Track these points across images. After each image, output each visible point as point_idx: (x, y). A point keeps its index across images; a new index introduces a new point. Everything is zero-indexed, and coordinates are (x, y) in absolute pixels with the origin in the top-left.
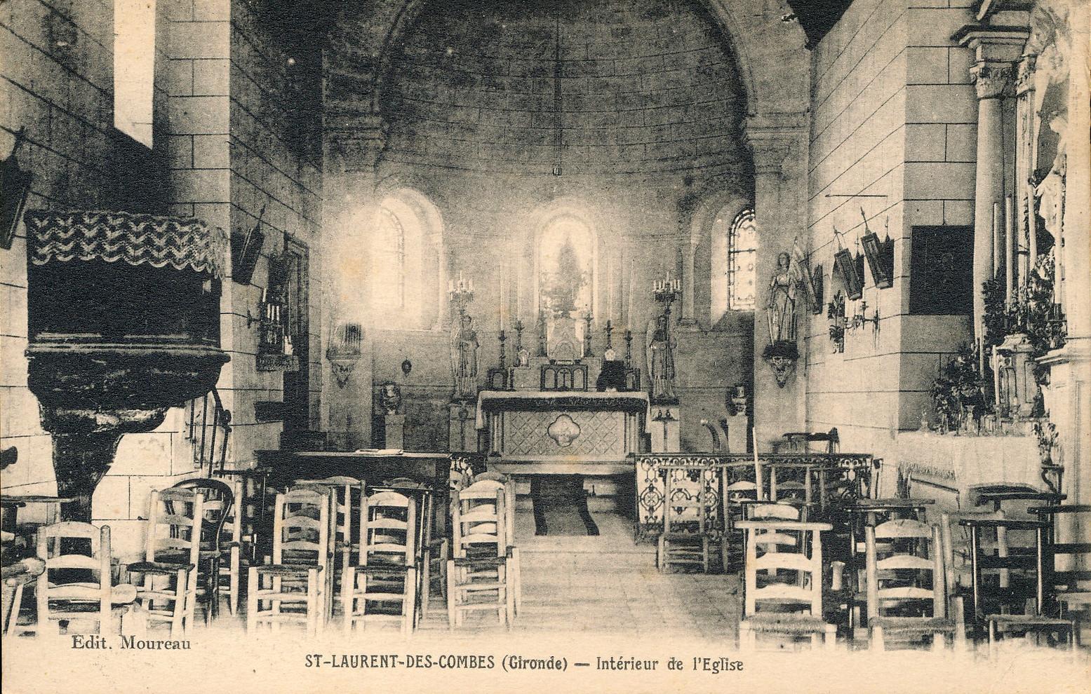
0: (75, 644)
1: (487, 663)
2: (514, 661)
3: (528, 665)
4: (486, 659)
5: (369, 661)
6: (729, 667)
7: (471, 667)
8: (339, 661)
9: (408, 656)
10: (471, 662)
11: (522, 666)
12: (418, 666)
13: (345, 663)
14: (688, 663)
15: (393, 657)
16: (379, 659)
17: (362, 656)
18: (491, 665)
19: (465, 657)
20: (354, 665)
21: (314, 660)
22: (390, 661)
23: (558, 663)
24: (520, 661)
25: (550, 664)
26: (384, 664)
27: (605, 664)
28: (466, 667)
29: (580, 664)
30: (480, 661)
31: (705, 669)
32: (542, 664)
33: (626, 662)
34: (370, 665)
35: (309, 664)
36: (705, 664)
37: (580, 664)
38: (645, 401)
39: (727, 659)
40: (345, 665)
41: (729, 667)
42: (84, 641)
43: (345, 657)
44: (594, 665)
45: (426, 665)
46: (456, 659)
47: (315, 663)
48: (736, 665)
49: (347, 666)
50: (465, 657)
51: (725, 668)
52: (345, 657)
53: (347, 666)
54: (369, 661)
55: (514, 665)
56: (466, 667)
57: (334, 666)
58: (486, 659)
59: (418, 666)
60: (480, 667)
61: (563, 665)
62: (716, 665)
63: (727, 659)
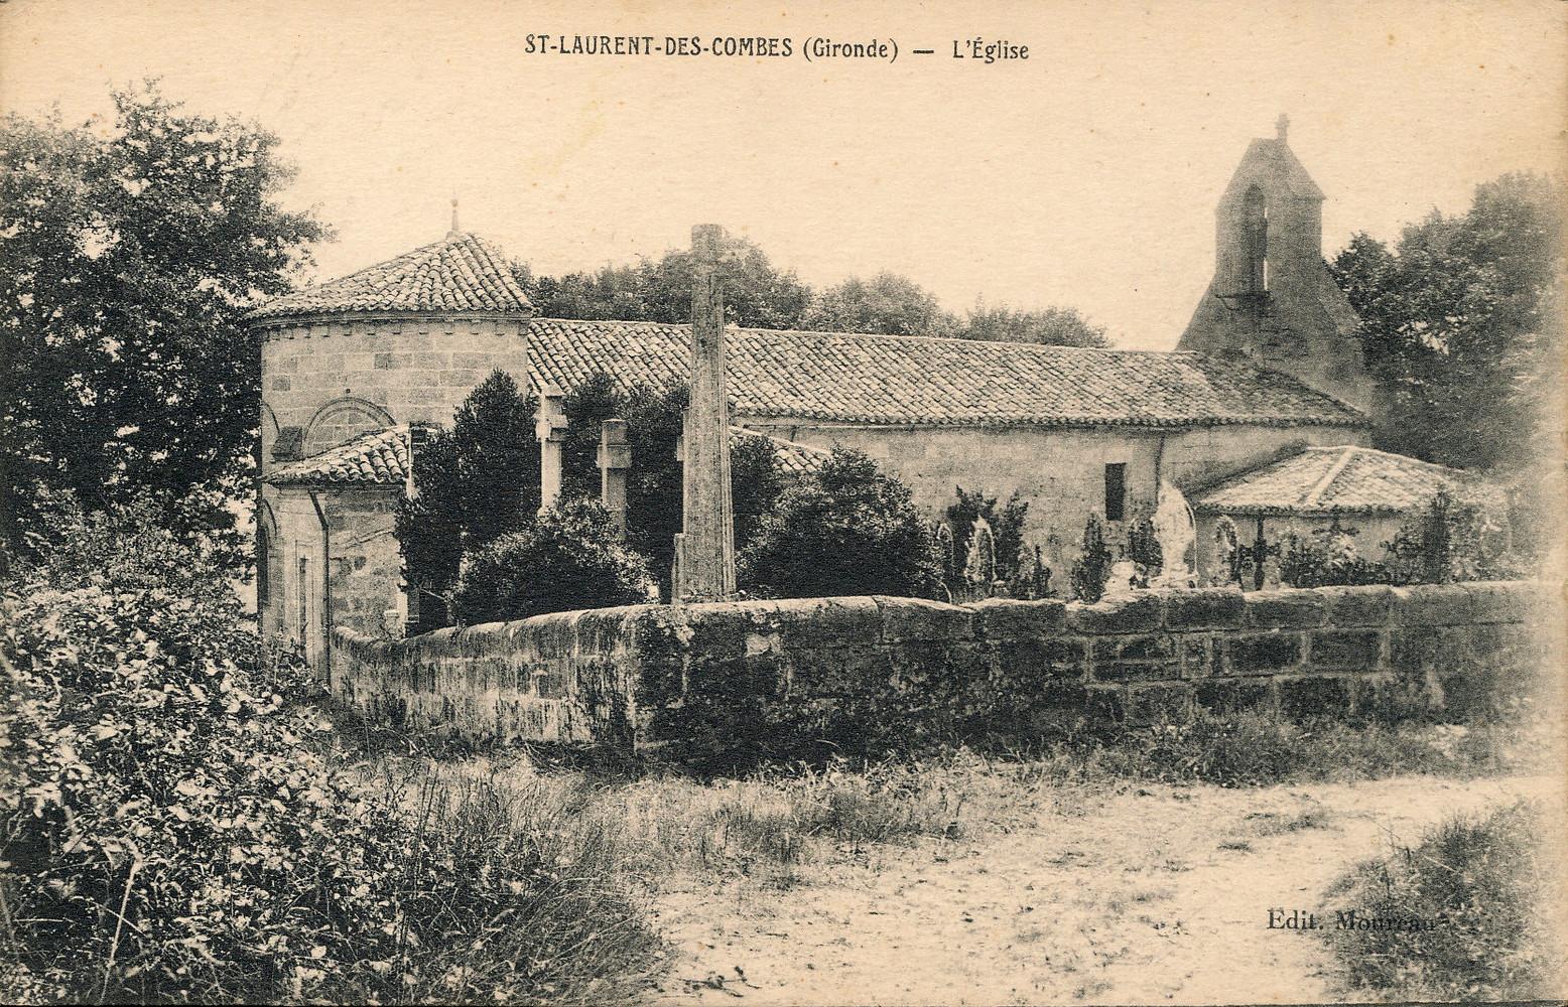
0: (1271, 922)
1: (781, 48)
2: (819, 44)
3: (839, 51)
4: (689, 43)
5: (612, 45)
6: (1010, 53)
7: (759, 54)
8: (569, 45)
9: (668, 39)
10: (759, 46)
11: (831, 53)
12: (680, 53)
13: (578, 47)
14: (945, 51)
15: (647, 39)
16: (626, 42)
17: (759, 39)
18: (787, 52)
19: (750, 40)
20: (591, 49)
21: (538, 42)
22: (642, 45)
23: (883, 48)
24: (828, 47)
25: (872, 49)
26: (633, 50)
27: (859, 49)
28: (751, 54)
29: (928, 52)
30: (771, 46)
31: (975, 56)
32: (859, 49)
33: (835, 46)
34: (613, 50)
35: (530, 49)
36: (976, 48)
37: (928, 52)
38: (1098, 599)
39: (1006, 42)
40: (578, 51)
41: (1010, 53)
42: (1284, 920)
43: (578, 38)
44: (905, 51)
45: (783, 53)
46: (738, 43)
47: (539, 48)
48: (1018, 51)
49: (581, 52)
50: (750, 40)
51: (1003, 55)
52: (578, 38)
53: (581, 52)
54: (612, 45)
55: (819, 52)
56: (751, 54)
57: (563, 51)
58: (689, 43)
59: (680, 53)
60: (771, 54)
61: (890, 52)
62: (990, 50)
63: (1006, 42)
